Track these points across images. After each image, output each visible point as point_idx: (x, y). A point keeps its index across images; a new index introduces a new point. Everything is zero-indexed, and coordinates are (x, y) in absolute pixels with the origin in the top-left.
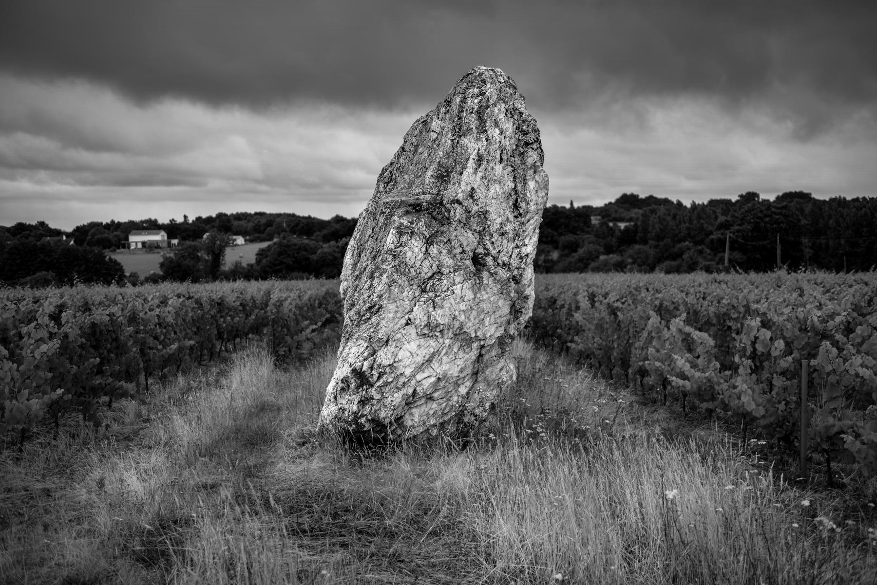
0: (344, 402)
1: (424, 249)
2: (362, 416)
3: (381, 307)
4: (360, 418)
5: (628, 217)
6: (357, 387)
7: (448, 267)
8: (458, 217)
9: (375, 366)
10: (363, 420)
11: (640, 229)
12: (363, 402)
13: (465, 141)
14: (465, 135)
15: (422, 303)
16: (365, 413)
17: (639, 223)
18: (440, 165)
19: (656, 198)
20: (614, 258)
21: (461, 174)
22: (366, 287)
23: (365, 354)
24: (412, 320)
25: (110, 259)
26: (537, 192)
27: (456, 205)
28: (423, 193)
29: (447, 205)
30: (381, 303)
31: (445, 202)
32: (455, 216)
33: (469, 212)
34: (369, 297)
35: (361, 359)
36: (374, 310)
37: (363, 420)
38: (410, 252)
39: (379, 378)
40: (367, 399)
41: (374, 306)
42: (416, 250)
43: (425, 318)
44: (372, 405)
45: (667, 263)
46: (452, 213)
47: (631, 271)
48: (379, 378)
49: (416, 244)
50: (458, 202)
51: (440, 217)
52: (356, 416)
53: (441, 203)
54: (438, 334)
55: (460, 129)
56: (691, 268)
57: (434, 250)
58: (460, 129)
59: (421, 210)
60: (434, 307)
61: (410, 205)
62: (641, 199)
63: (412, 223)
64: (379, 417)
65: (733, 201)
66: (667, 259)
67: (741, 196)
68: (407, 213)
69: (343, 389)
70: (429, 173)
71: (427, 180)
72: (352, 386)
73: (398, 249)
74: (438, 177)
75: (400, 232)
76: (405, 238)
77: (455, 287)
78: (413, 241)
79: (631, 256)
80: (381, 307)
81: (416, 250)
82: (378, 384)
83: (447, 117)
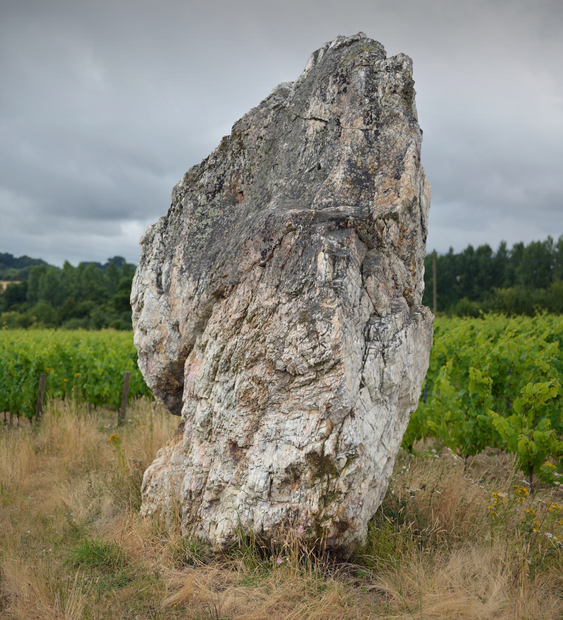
0: (296, 500)
2: (326, 518)
3: (338, 362)
4: (322, 521)
5: (5, 276)
7: (385, 306)
8: (392, 238)
10: (328, 524)
11: (30, 287)
12: (325, 500)
13: (389, 131)
14: (387, 123)
15: (373, 356)
17: (29, 281)
19: (29, 259)
20: (16, 315)
21: (398, 177)
25: (558, 246)
27: (391, 221)
30: (337, 357)
31: (375, 216)
32: (388, 236)
33: (404, 231)
36: (326, 367)
37: (328, 524)
39: (348, 464)
40: (332, 493)
41: (327, 361)
43: (378, 378)
44: (340, 502)
45: (73, 321)
47: (37, 327)
48: (348, 464)
50: (395, 217)
51: (370, 236)
52: (317, 520)
55: (378, 115)
56: (99, 325)
57: (371, 282)
58: (378, 115)
59: (346, 226)
60: (385, 362)
61: (332, 219)
62: (16, 259)
63: (343, 245)
64: (347, 518)
66: (72, 316)
68: (330, 230)
69: (286, 482)
72: (306, 476)
73: (337, 281)
74: (353, 182)
77: (399, 333)
79: (35, 314)
80: (338, 362)
82: (348, 472)
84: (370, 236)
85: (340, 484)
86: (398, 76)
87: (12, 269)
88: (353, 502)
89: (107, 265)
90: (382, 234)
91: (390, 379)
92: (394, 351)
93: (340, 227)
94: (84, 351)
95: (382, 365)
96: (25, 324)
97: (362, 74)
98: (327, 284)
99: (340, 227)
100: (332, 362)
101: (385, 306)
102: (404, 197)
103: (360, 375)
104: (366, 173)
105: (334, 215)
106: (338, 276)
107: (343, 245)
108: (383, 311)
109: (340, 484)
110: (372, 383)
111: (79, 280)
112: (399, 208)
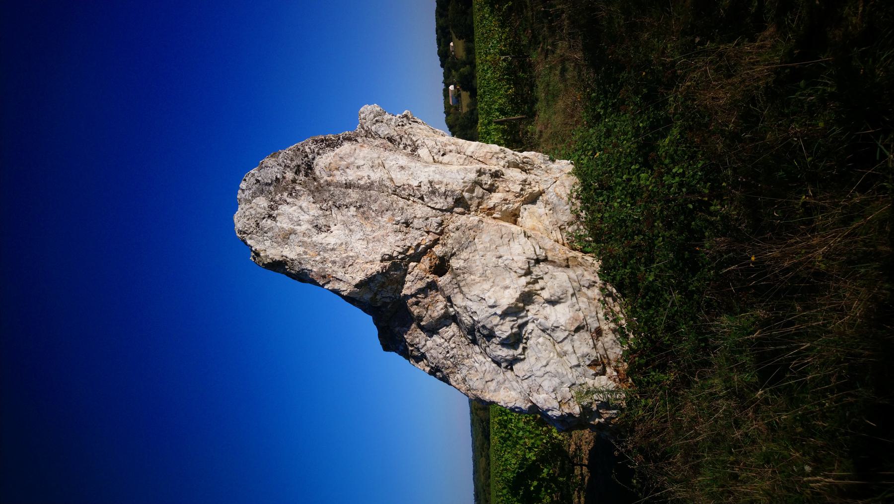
26: (358, 167)
32: (390, 297)
33: (384, 283)
38: (432, 351)
46: (388, 300)
90: (389, 303)
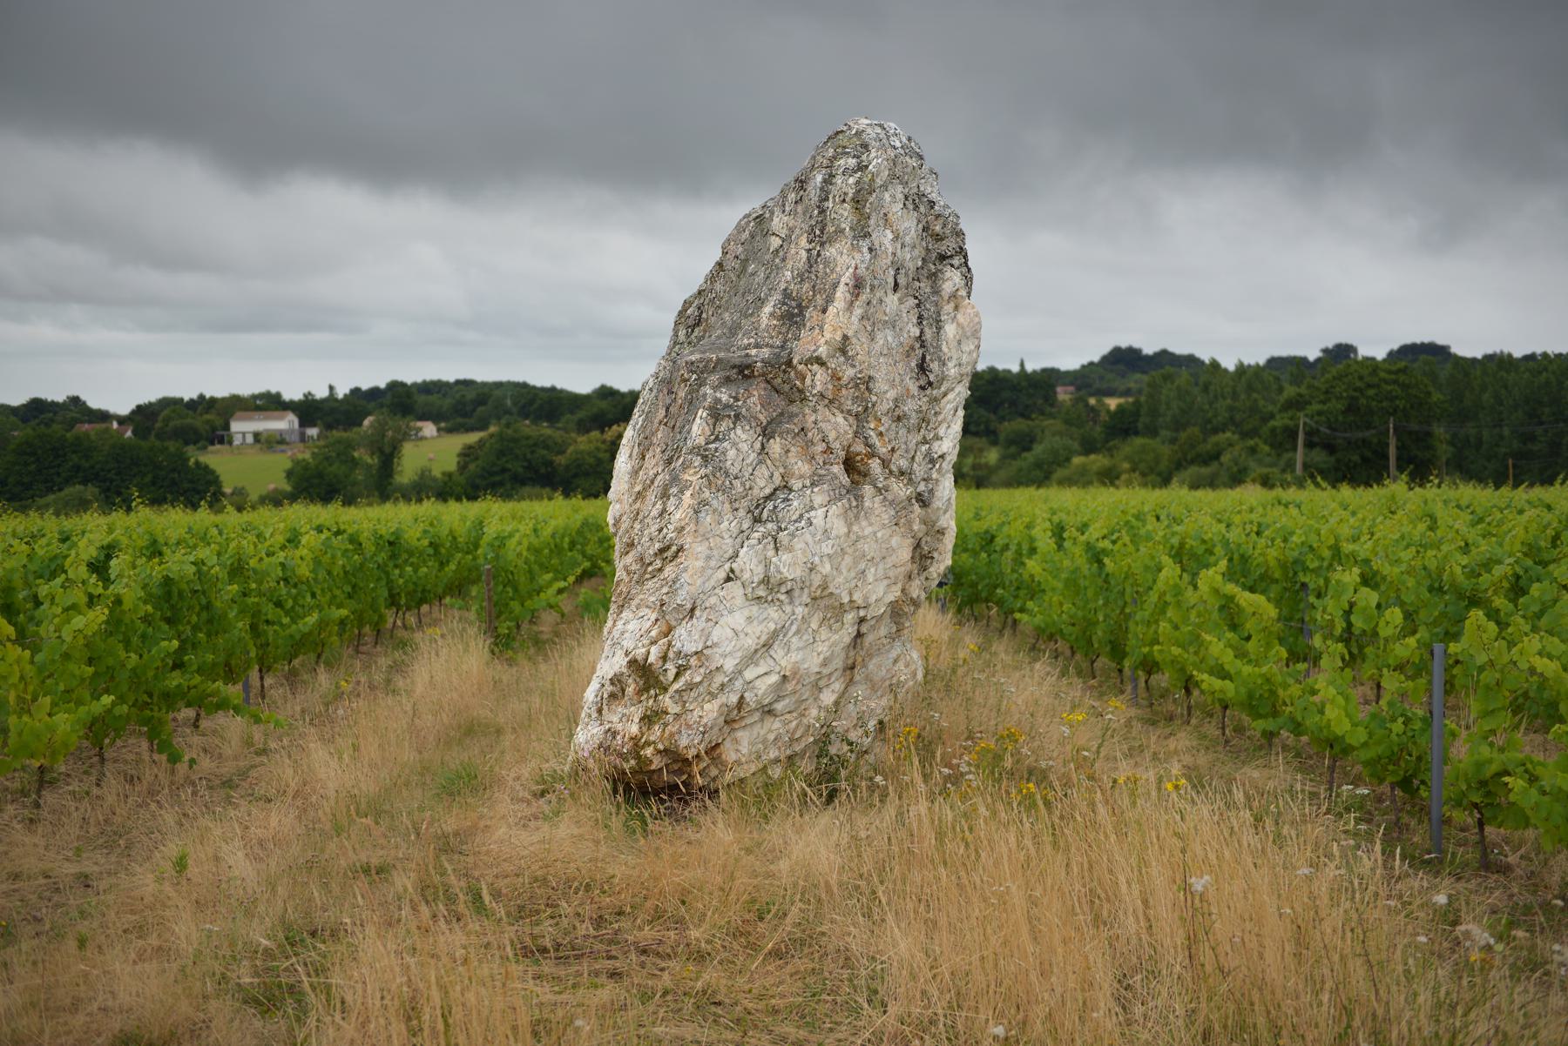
0: (615, 719)
1: (758, 446)
2: (648, 744)
6: (639, 693)
7: (801, 477)
8: (819, 388)
9: (671, 655)
10: (649, 751)
12: (648, 720)
13: (830, 252)
14: (830, 241)
16: (652, 738)
18: (786, 294)
19: (1172, 355)
20: (1098, 461)
21: (824, 311)
22: (655, 513)
23: (653, 633)
24: (737, 572)
27: (815, 367)
28: (757, 346)
29: (800, 367)
31: (795, 361)
34: (660, 530)
35: (646, 642)
36: (669, 554)
37: (649, 751)
39: (678, 675)
41: (669, 547)
42: (744, 447)
44: (666, 725)
45: (1193, 470)
46: (808, 381)
47: (1129, 484)
48: (678, 675)
49: (744, 437)
50: (821, 362)
53: (789, 363)
54: (783, 597)
57: (775, 446)
60: (777, 549)
61: (734, 367)
62: (1147, 357)
63: (736, 399)
65: (1312, 358)
66: (1192, 462)
67: (1325, 351)
68: (727, 380)
69: (612, 696)
70: (768, 309)
71: (764, 321)
72: (630, 690)
73: (712, 446)
74: (782, 317)
75: (716, 415)
76: (724, 426)
77: (813, 513)
78: (739, 431)
79: (1127, 458)
81: (744, 447)
82: (676, 686)
83: (799, 209)
84: (786, 387)
85: (666, 701)
86: (851, 180)
87: (1138, 376)
88: (689, 727)
89: (1318, 360)
91: (780, 572)
92: (793, 535)
93: (745, 376)
94: (413, 535)
95: (771, 553)
96: (1109, 477)
97: (819, 178)
98: (696, 450)
99: (745, 376)
100: (674, 548)
101: (801, 477)
102: (828, 335)
103: (727, 566)
104: (799, 306)
105: (737, 361)
106: (717, 439)
107: (736, 399)
108: (796, 484)
109: (666, 701)
110: (746, 576)
111: (1235, 395)
112: (823, 351)
